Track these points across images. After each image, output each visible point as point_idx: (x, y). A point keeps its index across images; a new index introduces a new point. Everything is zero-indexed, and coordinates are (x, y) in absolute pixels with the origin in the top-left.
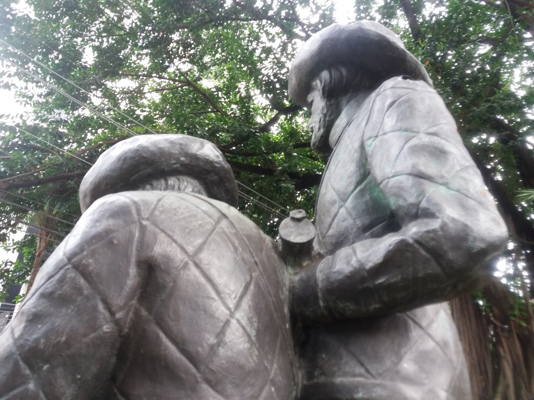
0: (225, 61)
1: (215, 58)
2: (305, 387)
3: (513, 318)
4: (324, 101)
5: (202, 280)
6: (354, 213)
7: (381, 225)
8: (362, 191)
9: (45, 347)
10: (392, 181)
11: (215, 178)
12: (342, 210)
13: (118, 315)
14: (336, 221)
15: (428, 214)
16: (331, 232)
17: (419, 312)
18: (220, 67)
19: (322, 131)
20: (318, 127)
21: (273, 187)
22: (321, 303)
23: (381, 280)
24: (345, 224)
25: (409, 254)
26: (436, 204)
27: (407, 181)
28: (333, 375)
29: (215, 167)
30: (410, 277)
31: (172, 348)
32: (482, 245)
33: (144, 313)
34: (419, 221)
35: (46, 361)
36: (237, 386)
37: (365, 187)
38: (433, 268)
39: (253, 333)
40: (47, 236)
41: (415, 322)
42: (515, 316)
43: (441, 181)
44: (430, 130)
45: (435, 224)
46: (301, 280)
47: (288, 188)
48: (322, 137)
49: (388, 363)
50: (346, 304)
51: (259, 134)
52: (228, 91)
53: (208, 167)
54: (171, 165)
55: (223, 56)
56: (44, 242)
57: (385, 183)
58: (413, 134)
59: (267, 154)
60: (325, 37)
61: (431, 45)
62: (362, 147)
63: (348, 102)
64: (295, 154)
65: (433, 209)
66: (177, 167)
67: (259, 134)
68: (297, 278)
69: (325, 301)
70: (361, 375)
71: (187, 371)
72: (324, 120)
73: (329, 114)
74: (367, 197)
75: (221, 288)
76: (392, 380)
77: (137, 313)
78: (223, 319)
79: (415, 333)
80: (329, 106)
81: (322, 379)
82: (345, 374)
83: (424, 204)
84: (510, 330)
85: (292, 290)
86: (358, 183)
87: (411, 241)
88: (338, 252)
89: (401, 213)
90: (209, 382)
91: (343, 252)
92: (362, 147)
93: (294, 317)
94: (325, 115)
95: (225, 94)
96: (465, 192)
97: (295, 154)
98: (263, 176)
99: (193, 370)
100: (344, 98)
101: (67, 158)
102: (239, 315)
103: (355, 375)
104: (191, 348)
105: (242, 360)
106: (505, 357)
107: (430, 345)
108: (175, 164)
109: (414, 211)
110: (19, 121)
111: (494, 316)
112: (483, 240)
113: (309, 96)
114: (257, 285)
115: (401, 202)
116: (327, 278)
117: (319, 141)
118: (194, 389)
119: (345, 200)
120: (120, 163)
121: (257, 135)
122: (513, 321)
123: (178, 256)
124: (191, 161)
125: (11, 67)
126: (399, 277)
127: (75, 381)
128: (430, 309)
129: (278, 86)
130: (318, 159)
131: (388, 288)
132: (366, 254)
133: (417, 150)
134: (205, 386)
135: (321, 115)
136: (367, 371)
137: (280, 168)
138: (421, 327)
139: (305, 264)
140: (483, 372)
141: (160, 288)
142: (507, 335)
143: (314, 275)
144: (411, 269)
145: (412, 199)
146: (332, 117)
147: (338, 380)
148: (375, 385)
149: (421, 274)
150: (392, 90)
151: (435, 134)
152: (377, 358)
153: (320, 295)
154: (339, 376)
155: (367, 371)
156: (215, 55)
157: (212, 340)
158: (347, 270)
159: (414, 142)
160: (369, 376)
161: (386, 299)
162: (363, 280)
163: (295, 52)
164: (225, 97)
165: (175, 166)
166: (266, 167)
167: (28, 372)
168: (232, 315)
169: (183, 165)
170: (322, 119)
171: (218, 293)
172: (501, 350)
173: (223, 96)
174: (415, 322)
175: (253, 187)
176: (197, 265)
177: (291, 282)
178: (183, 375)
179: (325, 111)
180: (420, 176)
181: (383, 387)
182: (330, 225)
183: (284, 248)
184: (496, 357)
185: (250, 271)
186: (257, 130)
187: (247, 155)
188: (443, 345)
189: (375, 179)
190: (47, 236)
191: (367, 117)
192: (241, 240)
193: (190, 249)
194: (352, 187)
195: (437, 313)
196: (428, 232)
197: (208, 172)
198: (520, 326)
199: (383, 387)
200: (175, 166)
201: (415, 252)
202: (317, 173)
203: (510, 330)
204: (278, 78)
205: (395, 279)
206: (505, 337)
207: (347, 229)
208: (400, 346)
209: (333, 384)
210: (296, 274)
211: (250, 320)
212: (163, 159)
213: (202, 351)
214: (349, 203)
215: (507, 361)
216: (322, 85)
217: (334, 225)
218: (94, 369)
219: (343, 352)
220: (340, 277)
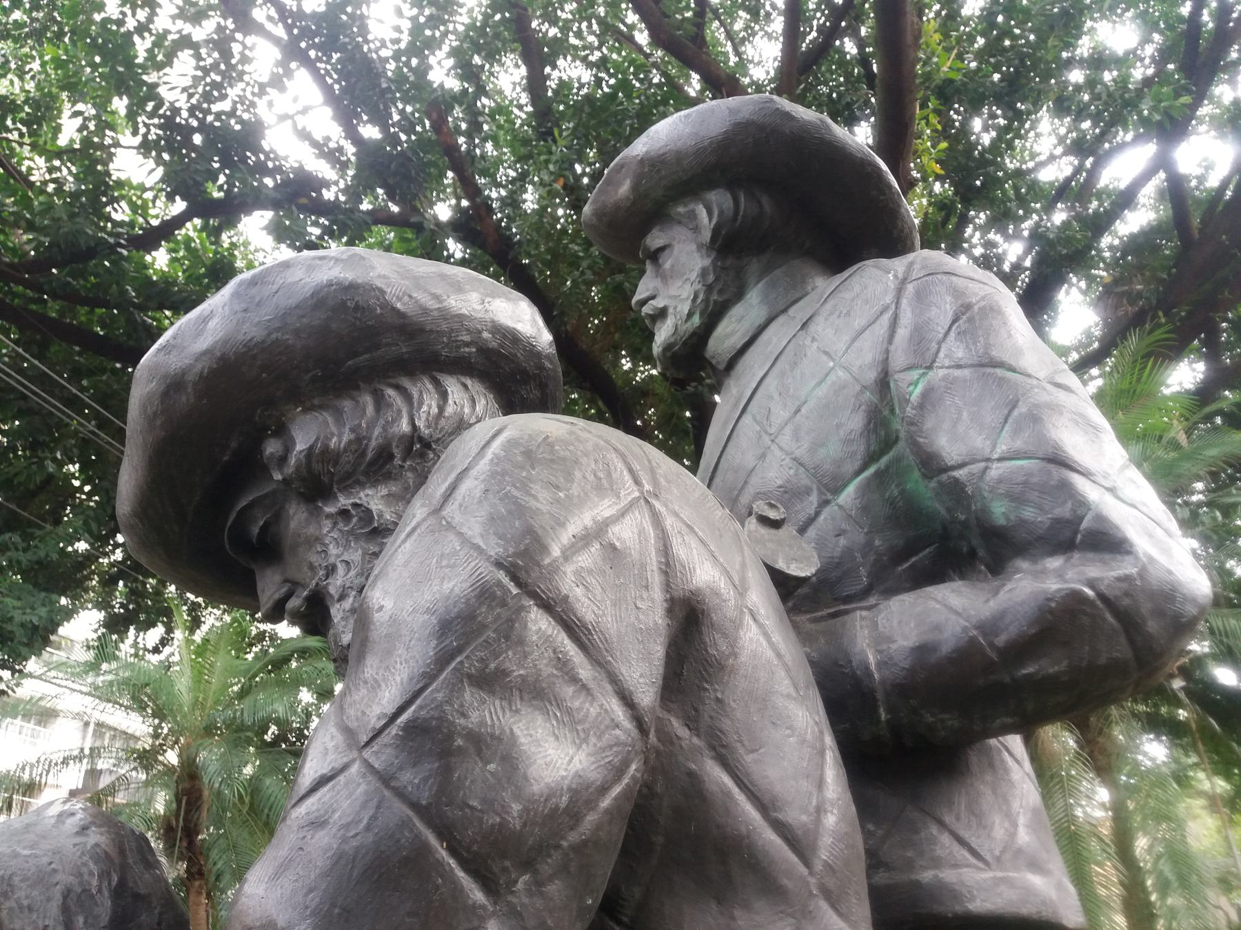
0: (38, 35)
1: (11, 20)
4: (708, 256)
7: (928, 550)
8: (879, 474)
9: (525, 825)
10: (996, 471)
18: (22, 47)
19: (696, 320)
20: (686, 312)
22: (883, 716)
23: (1029, 670)
25: (1085, 620)
28: (910, 865)
30: (1084, 664)
33: (678, 727)
35: (527, 865)
37: (888, 467)
45: (1126, 568)
48: (694, 334)
50: (941, 716)
51: (125, 252)
52: (36, 116)
53: (530, 366)
54: (459, 347)
55: (33, 20)
59: (143, 308)
61: (572, 145)
62: (883, 383)
63: (766, 271)
66: (470, 353)
67: (125, 252)
69: (890, 710)
72: (706, 300)
73: (720, 286)
80: (719, 270)
86: (871, 459)
92: (883, 383)
94: (709, 288)
95: (23, 122)
98: (118, 365)
100: (755, 260)
108: (467, 344)
110: (296, 165)
113: (655, 232)
117: (685, 343)
118: (807, 914)
119: (837, 491)
121: (121, 253)
124: (500, 345)
125: (1038, 131)
126: (1065, 663)
129: (197, 139)
135: (698, 287)
144: (1087, 648)
146: (726, 297)
147: (926, 876)
149: (1102, 660)
154: (926, 868)
156: (12, 12)
160: (980, 865)
163: (247, 68)
164: (24, 130)
165: (467, 350)
166: (131, 343)
167: (478, 895)
169: (484, 351)
170: (701, 297)
173: (19, 125)
175: (83, 389)
178: (785, 881)
179: (711, 278)
186: (122, 241)
187: (72, 298)
191: (886, 317)
194: (857, 464)
196: (1119, 579)
200: (467, 350)
204: (202, 122)
205: (1056, 668)
207: (848, 552)
209: (917, 884)
212: (444, 327)
214: (848, 496)
216: (714, 221)
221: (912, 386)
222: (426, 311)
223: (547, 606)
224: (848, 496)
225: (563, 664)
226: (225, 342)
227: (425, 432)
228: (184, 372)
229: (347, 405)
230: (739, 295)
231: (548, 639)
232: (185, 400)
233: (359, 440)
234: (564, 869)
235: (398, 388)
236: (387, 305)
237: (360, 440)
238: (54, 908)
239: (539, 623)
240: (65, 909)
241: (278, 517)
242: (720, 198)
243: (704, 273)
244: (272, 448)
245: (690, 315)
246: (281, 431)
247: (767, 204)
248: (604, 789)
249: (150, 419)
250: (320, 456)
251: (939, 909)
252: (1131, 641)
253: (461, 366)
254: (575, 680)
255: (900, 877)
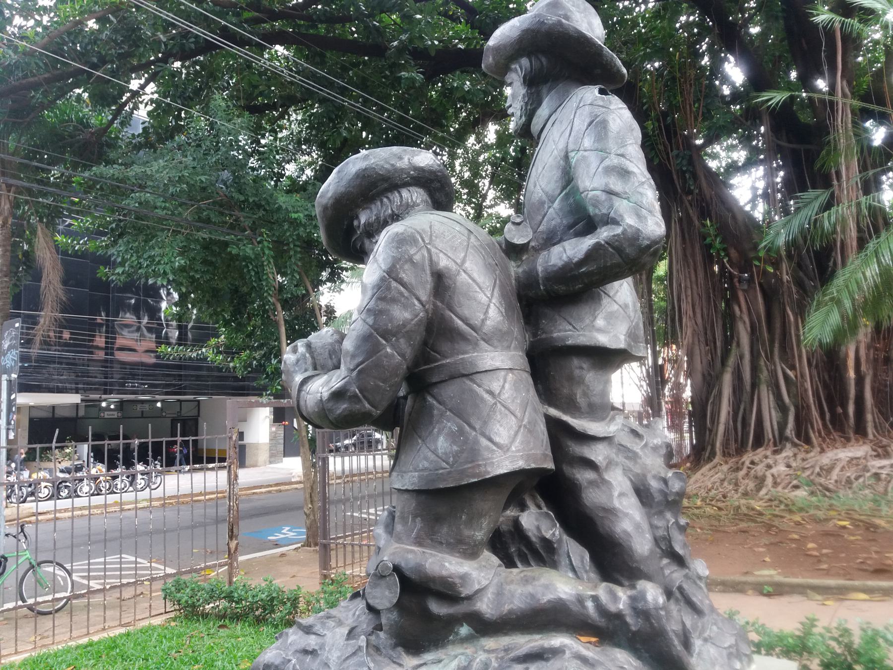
2: (531, 343)
3: (757, 263)
5: (470, 281)
6: (561, 214)
8: (566, 194)
10: (591, 194)
11: (438, 185)
12: (551, 210)
13: (427, 307)
14: (545, 219)
15: (615, 222)
16: (541, 228)
17: (608, 286)
19: (524, 119)
21: (386, 77)
24: (553, 223)
25: (601, 251)
26: (621, 216)
27: (603, 197)
28: (552, 332)
29: (437, 176)
31: (459, 322)
32: (647, 242)
33: (439, 304)
34: (609, 226)
35: (394, 336)
36: (499, 341)
38: (617, 259)
39: (503, 311)
40: (9, 191)
41: (605, 293)
42: (759, 259)
43: (624, 196)
44: (619, 152)
45: (619, 230)
46: (524, 272)
47: (413, 80)
49: (587, 321)
53: (432, 177)
56: (7, 201)
57: (585, 193)
58: (606, 155)
59: (371, 16)
60: (525, 26)
62: (566, 157)
63: (549, 91)
64: (418, 16)
65: (618, 219)
68: (520, 270)
69: (544, 285)
70: (570, 330)
71: (471, 335)
72: (526, 109)
74: (572, 200)
75: (481, 285)
76: (590, 331)
77: (434, 305)
78: (486, 303)
79: (605, 301)
81: (544, 336)
82: (560, 331)
83: (612, 215)
84: (751, 280)
85: (518, 279)
86: (564, 188)
87: (603, 242)
88: (552, 249)
89: (597, 219)
90: (484, 340)
91: (556, 250)
92: (566, 157)
93: (520, 298)
94: (526, 104)
96: (639, 203)
97: (418, 16)
99: (475, 334)
101: (25, 53)
102: (494, 301)
103: (566, 331)
104: (472, 322)
105: (500, 327)
106: (741, 318)
107: (616, 307)
109: (606, 219)
111: (729, 261)
112: (648, 239)
114: (500, 280)
115: (597, 211)
116: (545, 270)
119: (553, 202)
120: (359, 180)
122: (756, 266)
123: (454, 267)
127: (410, 345)
128: (616, 284)
130: (458, 18)
131: (587, 274)
132: (573, 252)
133: (609, 170)
134: (482, 342)
135: (522, 103)
136: (574, 327)
137: (395, 43)
138: (609, 296)
139: (524, 258)
140: (710, 342)
141: (447, 288)
142: (745, 287)
143: (535, 268)
145: (604, 211)
147: (555, 335)
148: (579, 335)
149: (609, 264)
150: (590, 107)
151: (622, 155)
152: (581, 320)
153: (541, 282)
155: (574, 327)
157: (482, 317)
158: (560, 263)
159: (607, 162)
161: (586, 281)
162: (571, 270)
167: (384, 342)
168: (490, 301)
169: (413, 178)
171: (480, 288)
172: (737, 309)
174: (605, 293)
176: (465, 271)
177: (516, 273)
179: (526, 99)
180: (610, 193)
181: (584, 335)
182: (541, 222)
183: (506, 245)
184: (729, 320)
185: (494, 271)
188: (625, 307)
189: (578, 189)
190: (9, 191)
191: (569, 128)
192: (484, 249)
193: (459, 261)
194: (559, 191)
195: (621, 285)
196: (614, 236)
197: (432, 181)
198: (765, 272)
199: (584, 335)
201: (606, 250)
202: (459, 46)
203: (751, 280)
206: (744, 291)
207: (555, 226)
208: (595, 311)
210: (518, 267)
211: (500, 302)
212: (397, 175)
213: (477, 322)
214: (556, 204)
215: (744, 323)
217: (544, 222)
218: (418, 338)
219: (557, 317)
220: (555, 269)
221: (574, 158)
222: (389, 171)
223: (396, 280)
224: (556, 204)
225: (402, 294)
226: (335, 193)
227: (396, 212)
228: (327, 204)
229: (373, 206)
230: (539, 104)
231: (396, 288)
232: (329, 212)
233: (377, 218)
234: (403, 337)
235: (388, 198)
236: (377, 173)
237: (378, 218)
238: (327, 353)
239: (394, 284)
240: (330, 354)
241: (363, 244)
242: (525, 61)
243: (524, 96)
244: (356, 223)
245: (521, 116)
246: (357, 217)
247: (544, 60)
248: (412, 320)
249: (322, 218)
250: (368, 225)
251: (556, 344)
252: (621, 257)
253: (406, 185)
254: (404, 296)
255: (549, 336)
